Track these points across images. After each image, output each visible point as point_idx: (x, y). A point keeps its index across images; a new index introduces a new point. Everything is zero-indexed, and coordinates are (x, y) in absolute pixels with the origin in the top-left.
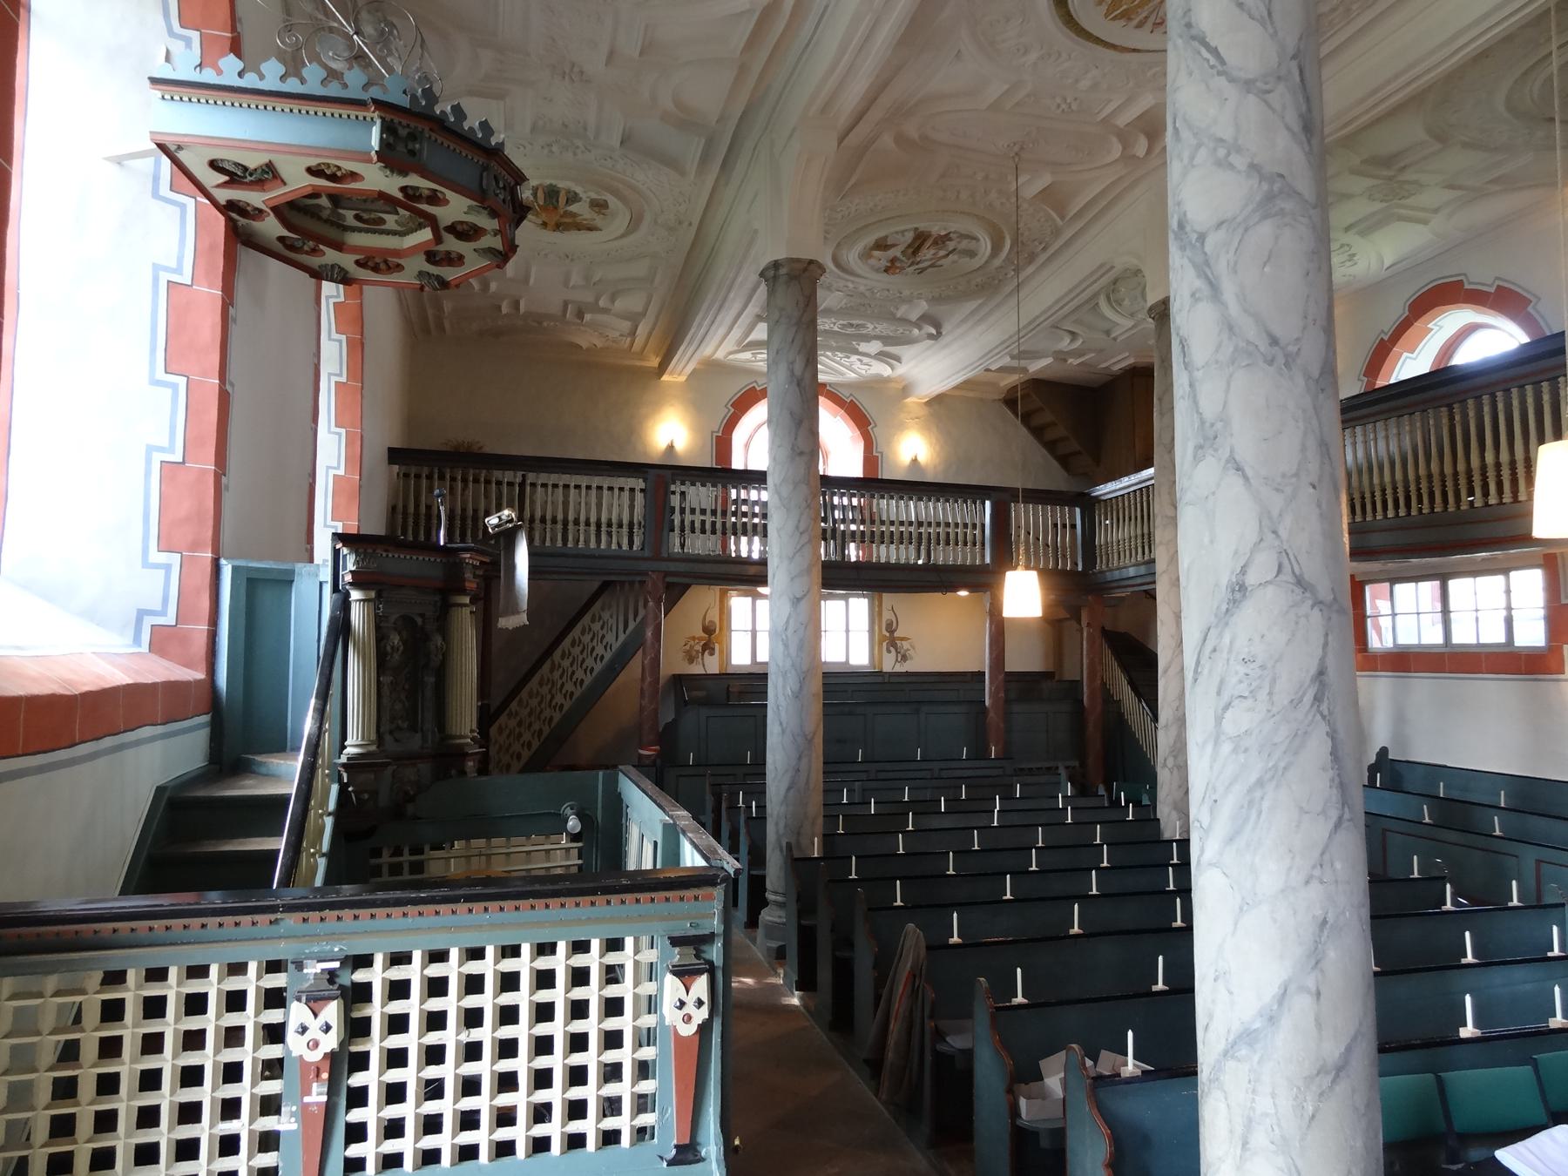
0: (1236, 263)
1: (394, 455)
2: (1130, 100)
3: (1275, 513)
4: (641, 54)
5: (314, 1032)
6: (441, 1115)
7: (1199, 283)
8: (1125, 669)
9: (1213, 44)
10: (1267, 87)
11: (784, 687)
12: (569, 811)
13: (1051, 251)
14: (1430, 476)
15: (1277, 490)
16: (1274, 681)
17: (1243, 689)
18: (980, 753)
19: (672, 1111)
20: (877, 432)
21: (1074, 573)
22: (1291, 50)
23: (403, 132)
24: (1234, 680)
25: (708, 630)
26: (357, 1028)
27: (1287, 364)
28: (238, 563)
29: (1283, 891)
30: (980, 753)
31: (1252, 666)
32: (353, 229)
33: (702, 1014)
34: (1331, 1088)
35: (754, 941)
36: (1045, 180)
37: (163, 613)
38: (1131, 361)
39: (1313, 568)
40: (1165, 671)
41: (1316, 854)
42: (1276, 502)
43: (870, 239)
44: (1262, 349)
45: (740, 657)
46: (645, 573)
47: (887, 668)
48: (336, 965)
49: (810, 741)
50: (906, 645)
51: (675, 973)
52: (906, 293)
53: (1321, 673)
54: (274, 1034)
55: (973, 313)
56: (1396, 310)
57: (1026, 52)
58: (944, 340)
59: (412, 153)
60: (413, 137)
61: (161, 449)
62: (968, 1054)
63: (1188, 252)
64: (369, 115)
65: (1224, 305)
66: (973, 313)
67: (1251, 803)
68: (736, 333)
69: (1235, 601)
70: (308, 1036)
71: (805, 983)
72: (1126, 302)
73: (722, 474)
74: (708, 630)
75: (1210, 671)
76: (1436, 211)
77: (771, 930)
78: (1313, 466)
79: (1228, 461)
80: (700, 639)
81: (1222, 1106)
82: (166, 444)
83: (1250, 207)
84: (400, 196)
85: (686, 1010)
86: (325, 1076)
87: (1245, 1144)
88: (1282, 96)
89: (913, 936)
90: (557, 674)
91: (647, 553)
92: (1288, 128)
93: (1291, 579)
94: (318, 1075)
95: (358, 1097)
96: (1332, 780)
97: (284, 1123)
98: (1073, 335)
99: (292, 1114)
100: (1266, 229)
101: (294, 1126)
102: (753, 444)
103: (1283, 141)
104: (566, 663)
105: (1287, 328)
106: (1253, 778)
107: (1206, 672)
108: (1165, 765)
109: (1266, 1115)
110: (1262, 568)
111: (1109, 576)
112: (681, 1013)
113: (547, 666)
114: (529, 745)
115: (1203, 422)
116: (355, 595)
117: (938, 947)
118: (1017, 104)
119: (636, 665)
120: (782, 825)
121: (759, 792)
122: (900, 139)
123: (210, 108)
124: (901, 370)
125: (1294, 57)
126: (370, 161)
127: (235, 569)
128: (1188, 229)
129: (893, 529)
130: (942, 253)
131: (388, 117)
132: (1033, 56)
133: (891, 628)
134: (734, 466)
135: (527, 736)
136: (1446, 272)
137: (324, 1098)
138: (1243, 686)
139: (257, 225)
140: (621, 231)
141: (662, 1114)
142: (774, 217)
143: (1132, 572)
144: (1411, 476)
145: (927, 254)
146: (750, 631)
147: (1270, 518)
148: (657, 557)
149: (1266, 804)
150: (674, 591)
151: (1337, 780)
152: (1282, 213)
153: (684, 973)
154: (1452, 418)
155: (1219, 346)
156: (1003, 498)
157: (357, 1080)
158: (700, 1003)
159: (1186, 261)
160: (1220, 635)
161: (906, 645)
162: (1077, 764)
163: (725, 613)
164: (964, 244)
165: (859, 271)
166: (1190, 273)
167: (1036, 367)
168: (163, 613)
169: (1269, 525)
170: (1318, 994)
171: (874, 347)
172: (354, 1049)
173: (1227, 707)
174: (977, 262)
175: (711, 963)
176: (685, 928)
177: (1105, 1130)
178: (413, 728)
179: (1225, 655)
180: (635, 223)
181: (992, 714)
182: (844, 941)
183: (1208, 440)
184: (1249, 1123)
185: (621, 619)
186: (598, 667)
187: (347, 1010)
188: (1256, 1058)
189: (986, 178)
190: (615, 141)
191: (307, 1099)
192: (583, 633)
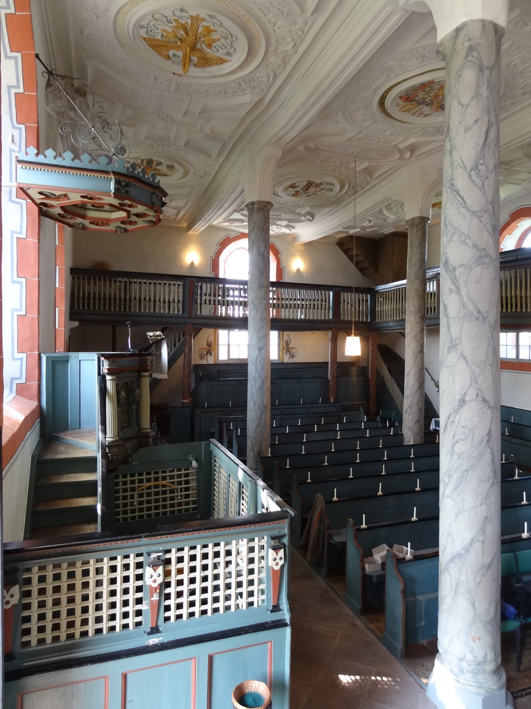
0: (467, 281)
1: (71, 269)
2: (406, 139)
3: (477, 375)
4: (199, 114)
5: (155, 577)
6: (195, 601)
7: (452, 286)
8: (385, 361)
9: (462, 195)
10: (481, 215)
11: (255, 385)
12: (192, 459)
13: (364, 190)
14: (516, 297)
15: (478, 367)
16: (473, 435)
17: (462, 437)
18: (326, 400)
19: (271, 594)
20: (282, 257)
21: (366, 322)
23: (123, 184)
24: (459, 433)
25: (209, 345)
26: (167, 574)
29: (473, 507)
30: (326, 400)
32: (90, 209)
33: (282, 562)
34: (486, 573)
36: (366, 165)
37: (20, 378)
38: (393, 230)
40: (408, 374)
41: (485, 495)
42: (477, 371)
43: (289, 183)
44: (475, 314)
45: (223, 356)
46: (185, 324)
48: (161, 554)
49: (266, 407)
50: (294, 351)
51: (273, 549)
52: (301, 204)
53: (490, 432)
54: (139, 577)
55: (328, 212)
57: (365, 121)
58: (314, 221)
59: (127, 192)
60: (127, 185)
62: (344, 545)
63: (449, 273)
64: (109, 177)
66: (328, 212)
67: (463, 477)
68: (224, 215)
69: (461, 406)
70: (153, 578)
72: (394, 209)
74: (209, 345)
75: (451, 429)
76: (524, 181)
79: (460, 355)
80: (206, 349)
81: (448, 578)
82: (18, 307)
83: (473, 261)
84: (118, 205)
85: (276, 561)
86: (158, 591)
87: (456, 591)
88: (486, 218)
89: (320, 498)
92: (488, 231)
93: (481, 399)
94: (156, 591)
96: (491, 469)
97: (143, 607)
98: (370, 221)
99: (147, 604)
100: (478, 269)
101: (147, 608)
103: (486, 235)
106: (465, 468)
107: (449, 429)
108: (406, 412)
109: (463, 582)
110: (471, 395)
111: (381, 325)
112: (275, 562)
115: (452, 339)
116: (108, 378)
117: (329, 502)
118: (359, 139)
120: (254, 441)
122: (307, 148)
123: (39, 172)
124: (293, 231)
125: (491, 203)
126: (110, 196)
127: (47, 358)
128: (449, 264)
130: (318, 189)
131: (118, 178)
132: (367, 123)
133: (287, 344)
137: (158, 598)
138: (463, 436)
139: (51, 210)
140: (179, 177)
141: (268, 595)
142: (249, 178)
143: (391, 324)
144: (509, 296)
145: (312, 190)
147: (475, 377)
148: (190, 317)
149: (469, 478)
150: (197, 331)
152: (484, 263)
153: (276, 549)
154: (526, 274)
155: (459, 311)
156: (338, 290)
157: (167, 591)
158: (281, 558)
159: (448, 277)
160: (455, 417)
161: (294, 351)
162: (365, 402)
163: (216, 337)
164: (328, 187)
165: (282, 196)
166: (449, 282)
167: (351, 232)
168: (20, 378)
169: (474, 379)
170: (483, 542)
171: (284, 223)
172: (166, 581)
173: (456, 442)
174: (333, 193)
175: (284, 544)
176: (276, 533)
177: (402, 580)
178: (129, 427)
179: (456, 424)
180: (186, 173)
181: (331, 383)
183: (453, 346)
184: (458, 584)
185: (173, 342)
187: (164, 568)
188: (461, 563)
189: (341, 163)
190: (182, 144)
191: (152, 599)
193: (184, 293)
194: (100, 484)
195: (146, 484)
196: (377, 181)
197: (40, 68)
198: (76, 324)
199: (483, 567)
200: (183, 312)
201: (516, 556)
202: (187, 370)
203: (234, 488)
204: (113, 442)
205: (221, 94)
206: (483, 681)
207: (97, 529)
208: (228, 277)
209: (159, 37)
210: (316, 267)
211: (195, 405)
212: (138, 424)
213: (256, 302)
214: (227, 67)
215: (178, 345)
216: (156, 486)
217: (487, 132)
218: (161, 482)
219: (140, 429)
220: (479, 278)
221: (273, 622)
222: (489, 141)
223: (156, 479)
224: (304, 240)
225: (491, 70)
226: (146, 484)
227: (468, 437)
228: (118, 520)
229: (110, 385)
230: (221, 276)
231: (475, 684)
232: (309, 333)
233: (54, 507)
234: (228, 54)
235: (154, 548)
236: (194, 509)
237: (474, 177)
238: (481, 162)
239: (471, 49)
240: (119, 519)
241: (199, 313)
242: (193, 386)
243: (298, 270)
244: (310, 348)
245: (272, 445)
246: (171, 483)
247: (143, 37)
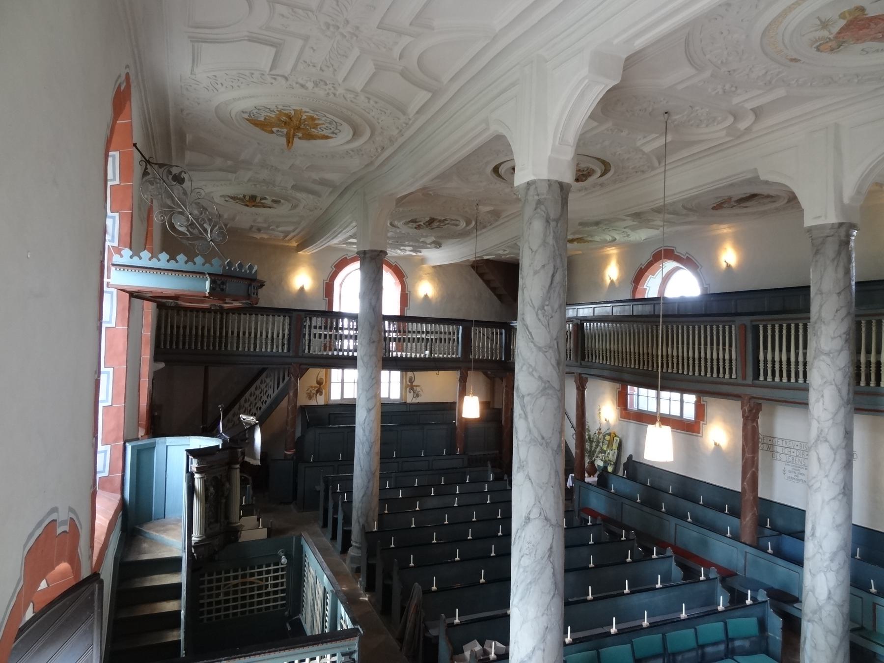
7: (521, 412)
13: (493, 226)
17: (527, 552)
18: (451, 452)
20: (408, 281)
21: (500, 361)
22: (555, 337)
23: (219, 282)
25: (320, 383)
30: (451, 452)
35: (345, 561)
39: (551, 515)
42: (541, 492)
45: (335, 395)
47: (409, 400)
49: (374, 474)
53: (551, 548)
56: (647, 257)
60: (223, 283)
62: (437, 637)
65: (528, 423)
71: (370, 588)
73: (331, 316)
74: (320, 383)
77: (353, 559)
78: (553, 480)
80: (315, 387)
89: (417, 588)
91: (291, 354)
100: (543, 399)
102: (348, 292)
105: (547, 434)
110: (535, 514)
116: (197, 476)
117: (427, 591)
119: (284, 403)
121: (350, 493)
127: (132, 447)
129: (424, 336)
133: (411, 381)
134: (334, 310)
136: (669, 244)
145: (436, 224)
146: (344, 385)
150: (302, 373)
152: (548, 394)
156: (467, 324)
167: (486, 257)
169: (538, 499)
176: (347, 650)
178: (217, 521)
182: (388, 575)
186: (264, 407)
192: (256, 389)
193: (290, 324)
194: (184, 588)
196: (506, 219)
197: (137, 156)
198: (162, 365)
200: (289, 350)
201: (598, 654)
203: (320, 591)
204: (199, 542)
207: (179, 636)
208: (344, 310)
209: (262, 119)
210: (447, 296)
211: (300, 457)
212: (227, 517)
213: (366, 359)
214: (332, 143)
215: (281, 385)
216: (244, 584)
217: (553, 276)
222: (555, 284)
223: (244, 576)
224: (424, 281)
225: (557, 222)
229: (198, 484)
230: (335, 309)
232: (434, 373)
234: (333, 133)
236: (282, 605)
237: (541, 316)
238: (547, 303)
239: (539, 203)
240: (203, 619)
241: (306, 351)
242: (298, 434)
243: (426, 296)
244: (436, 386)
245: (381, 516)
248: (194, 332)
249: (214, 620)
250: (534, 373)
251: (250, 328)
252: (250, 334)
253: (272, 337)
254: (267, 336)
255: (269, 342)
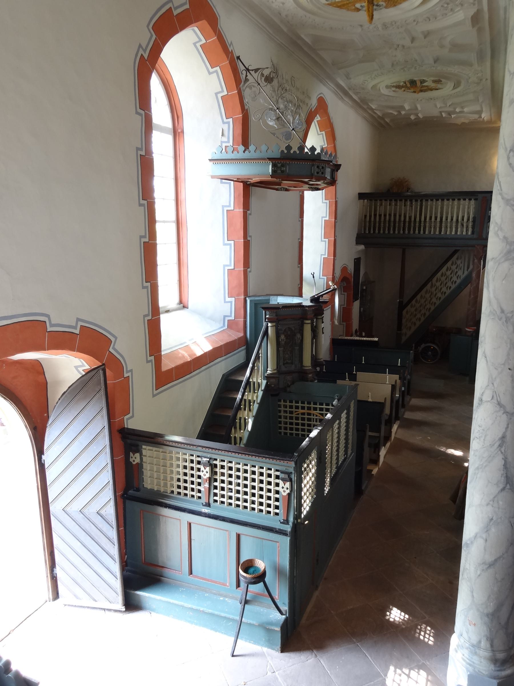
3: (494, 377)
12: (336, 397)
15: (496, 369)
23: (279, 165)
27: (506, 321)
28: (253, 298)
31: (481, 428)
37: (231, 316)
41: (492, 497)
53: (503, 437)
61: (227, 266)
82: (229, 264)
83: (502, 255)
90: (434, 289)
91: (475, 236)
93: (496, 402)
95: (216, 487)
96: (502, 475)
97: (201, 488)
104: (438, 284)
113: (429, 285)
114: (420, 319)
116: (269, 325)
119: (466, 291)
123: (224, 165)
135: (418, 316)
147: (492, 378)
149: (479, 476)
151: (505, 475)
168: (231, 316)
186: (453, 287)
192: (447, 270)
195: (301, 411)
198: (362, 247)
199: (484, 563)
200: (473, 233)
202: (472, 296)
205: (431, 19)
206: (477, 662)
218: (312, 412)
219: (302, 366)
220: (506, 275)
221: (279, 529)
226: (301, 411)
227: (482, 437)
228: (280, 433)
231: (468, 661)
233: (225, 414)
235: (205, 455)
246: (320, 414)
247: (326, 4)
248: (402, 219)
249: (294, 435)
250: (500, 233)
251: (436, 214)
252: (436, 218)
253: (457, 220)
254: (452, 220)
255: (454, 225)
